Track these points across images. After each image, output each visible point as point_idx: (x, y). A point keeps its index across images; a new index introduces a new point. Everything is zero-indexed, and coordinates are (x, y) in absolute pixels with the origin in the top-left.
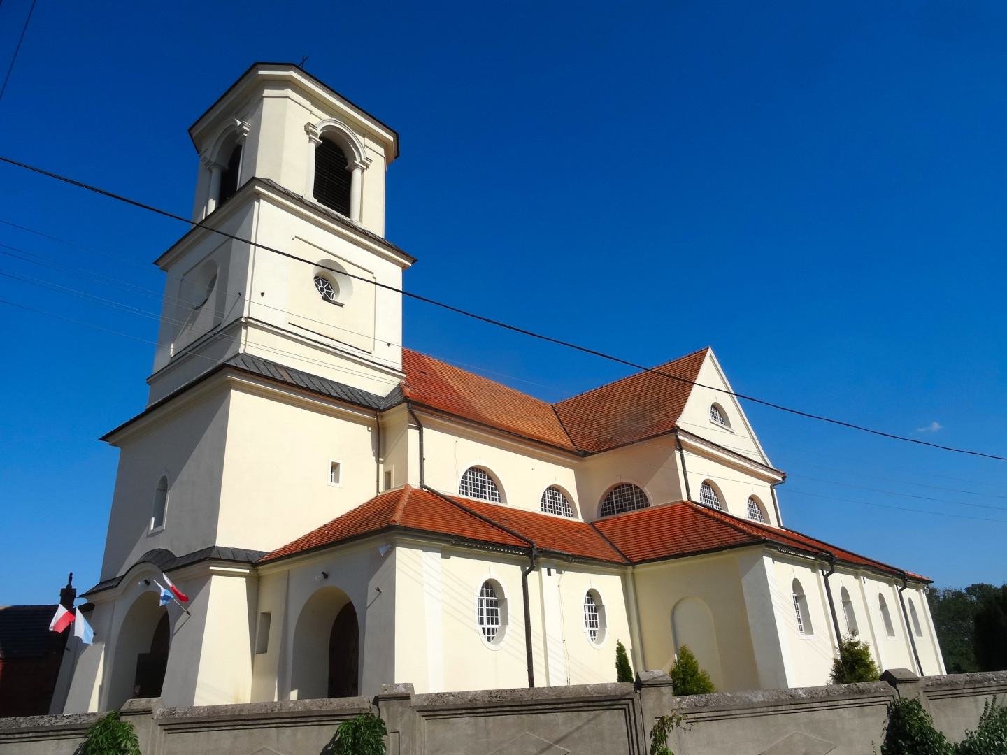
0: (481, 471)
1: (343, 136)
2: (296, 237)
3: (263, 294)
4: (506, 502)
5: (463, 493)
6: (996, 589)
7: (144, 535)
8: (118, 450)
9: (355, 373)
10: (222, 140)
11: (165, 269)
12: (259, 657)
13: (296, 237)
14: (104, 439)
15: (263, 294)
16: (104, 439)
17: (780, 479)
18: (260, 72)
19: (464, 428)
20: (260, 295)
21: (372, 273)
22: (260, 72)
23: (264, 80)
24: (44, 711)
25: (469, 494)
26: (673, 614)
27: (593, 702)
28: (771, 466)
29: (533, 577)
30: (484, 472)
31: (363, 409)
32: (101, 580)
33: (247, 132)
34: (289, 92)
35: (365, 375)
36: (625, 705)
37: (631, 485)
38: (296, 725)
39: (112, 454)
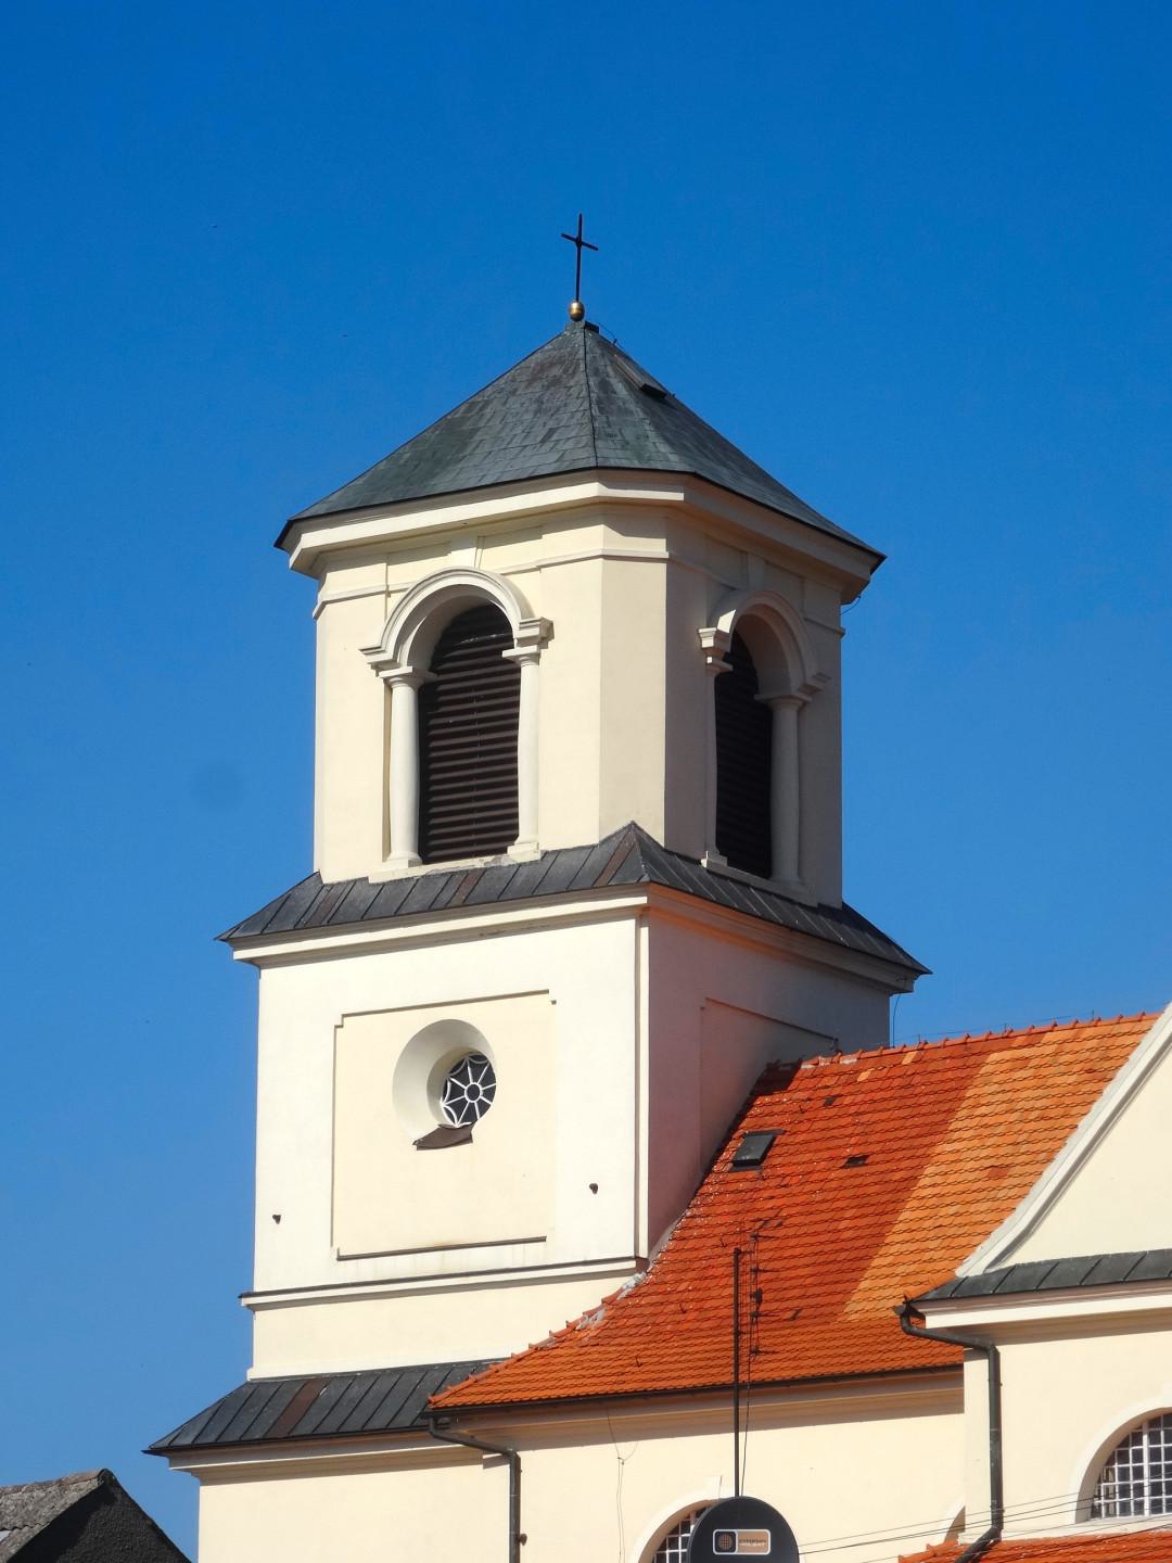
2: (344, 1016)
21: (547, 992)
23: (321, 552)
29: (389, 567)
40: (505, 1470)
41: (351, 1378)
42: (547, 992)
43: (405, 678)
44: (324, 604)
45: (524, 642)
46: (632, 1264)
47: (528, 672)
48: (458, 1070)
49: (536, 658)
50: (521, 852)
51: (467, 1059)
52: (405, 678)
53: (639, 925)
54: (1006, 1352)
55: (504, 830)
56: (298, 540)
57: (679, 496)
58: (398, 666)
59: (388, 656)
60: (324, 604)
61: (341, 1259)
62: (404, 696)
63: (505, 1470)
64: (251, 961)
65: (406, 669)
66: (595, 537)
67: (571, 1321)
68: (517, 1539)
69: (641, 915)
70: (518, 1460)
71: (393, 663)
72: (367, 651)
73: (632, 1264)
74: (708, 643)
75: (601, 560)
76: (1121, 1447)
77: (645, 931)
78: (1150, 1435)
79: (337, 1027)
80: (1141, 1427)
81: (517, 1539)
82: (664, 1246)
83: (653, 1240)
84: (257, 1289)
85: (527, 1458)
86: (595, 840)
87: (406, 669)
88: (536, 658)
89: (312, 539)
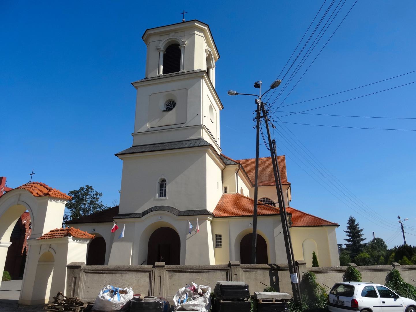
6: (408, 246)
7: (153, 199)
8: (122, 161)
10: (167, 42)
11: (136, 88)
12: (218, 249)
14: (116, 155)
16: (116, 155)
18: (196, 24)
22: (196, 24)
23: (195, 27)
24: (103, 264)
26: (303, 243)
27: (283, 268)
32: (335, 232)
33: (185, 45)
36: (226, 271)
37: (268, 199)
38: (381, 271)
39: (119, 162)
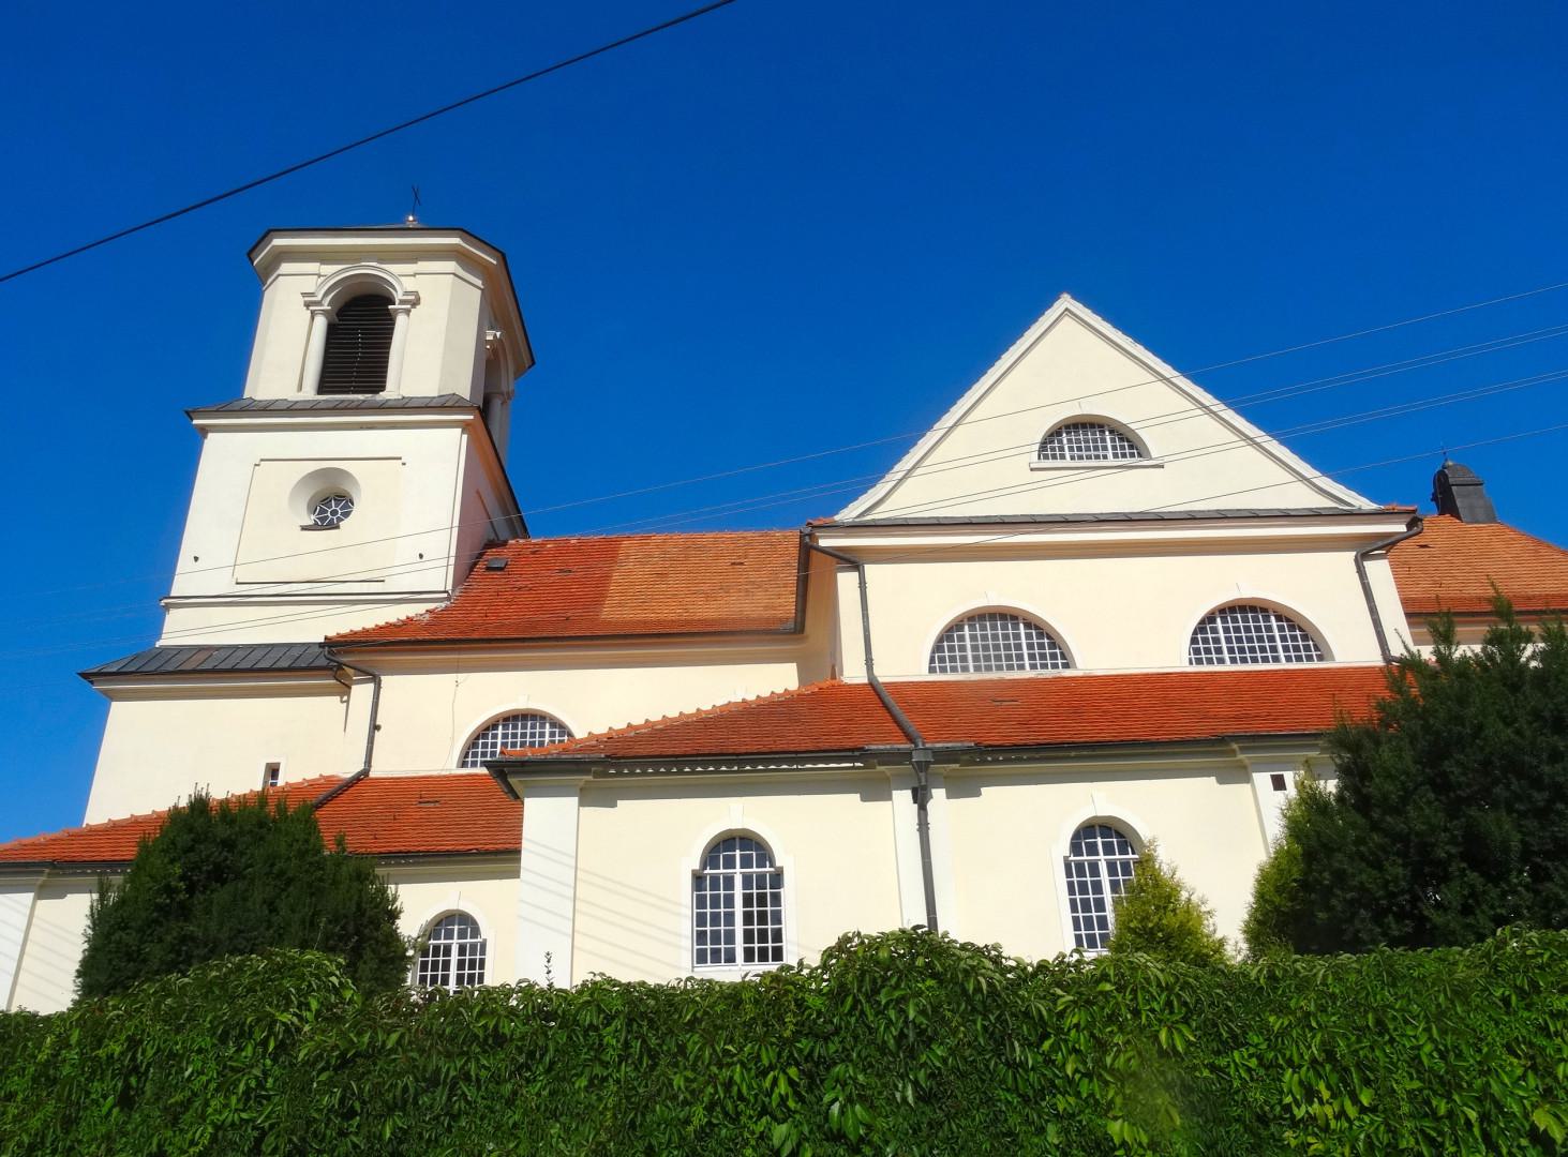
0: (1253, 609)
1: (369, 280)
2: (262, 460)
3: (196, 559)
4: (1333, 659)
5: (1199, 661)
9: (1046, 483)
13: (262, 460)
15: (196, 559)
17: (1402, 528)
19: (456, 656)
20: (199, 561)
21: (400, 459)
23: (281, 253)
25: (1283, 659)
28: (1366, 504)
29: (41, 903)
30: (1264, 610)
31: (256, 674)
34: (285, 268)
35: (1035, 486)
40: (371, 686)
41: (236, 648)
42: (400, 459)
43: (325, 312)
44: (279, 275)
45: (402, 302)
46: (445, 595)
47: (401, 320)
48: (326, 501)
49: (408, 312)
50: (383, 396)
51: (332, 496)
52: (325, 312)
53: (463, 433)
54: (869, 569)
55: (380, 386)
56: (271, 241)
57: (495, 262)
58: (322, 305)
59: (319, 298)
60: (279, 275)
61: (237, 583)
62: (321, 323)
63: (371, 686)
64: (105, 692)
65: (326, 307)
66: (451, 266)
67: (410, 615)
68: (375, 727)
69: (466, 427)
70: (380, 681)
71: (319, 303)
72: (304, 295)
73: (445, 595)
74: (490, 338)
75: (452, 276)
76: (951, 631)
77: (465, 437)
78: (970, 626)
79: (256, 465)
80: (962, 621)
81: (375, 727)
82: (457, 594)
83: (455, 585)
84: (172, 595)
85: (386, 680)
86: (436, 395)
87: (326, 307)
88: (408, 312)
89: (278, 242)
